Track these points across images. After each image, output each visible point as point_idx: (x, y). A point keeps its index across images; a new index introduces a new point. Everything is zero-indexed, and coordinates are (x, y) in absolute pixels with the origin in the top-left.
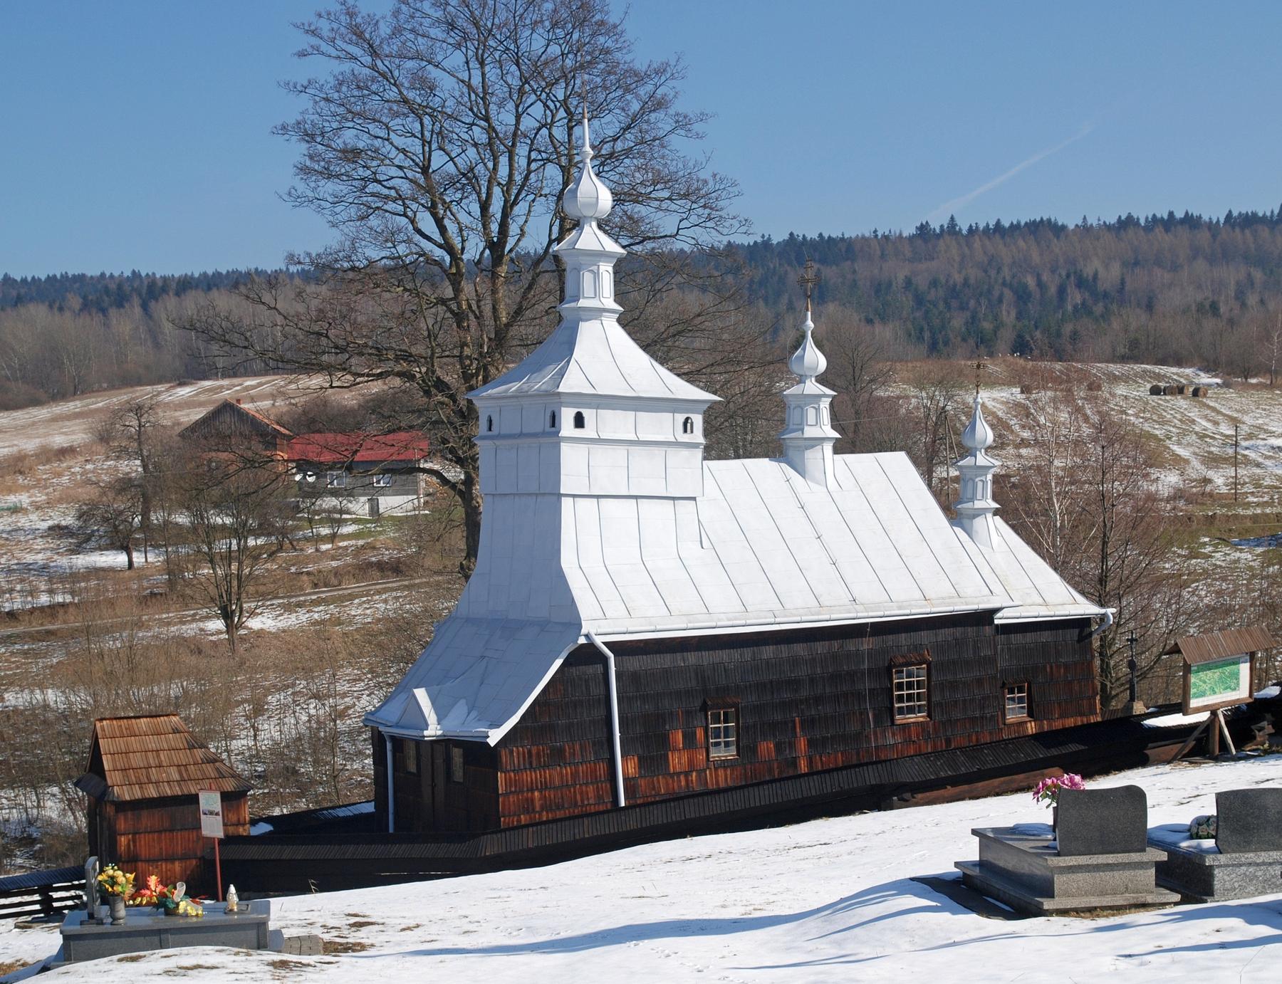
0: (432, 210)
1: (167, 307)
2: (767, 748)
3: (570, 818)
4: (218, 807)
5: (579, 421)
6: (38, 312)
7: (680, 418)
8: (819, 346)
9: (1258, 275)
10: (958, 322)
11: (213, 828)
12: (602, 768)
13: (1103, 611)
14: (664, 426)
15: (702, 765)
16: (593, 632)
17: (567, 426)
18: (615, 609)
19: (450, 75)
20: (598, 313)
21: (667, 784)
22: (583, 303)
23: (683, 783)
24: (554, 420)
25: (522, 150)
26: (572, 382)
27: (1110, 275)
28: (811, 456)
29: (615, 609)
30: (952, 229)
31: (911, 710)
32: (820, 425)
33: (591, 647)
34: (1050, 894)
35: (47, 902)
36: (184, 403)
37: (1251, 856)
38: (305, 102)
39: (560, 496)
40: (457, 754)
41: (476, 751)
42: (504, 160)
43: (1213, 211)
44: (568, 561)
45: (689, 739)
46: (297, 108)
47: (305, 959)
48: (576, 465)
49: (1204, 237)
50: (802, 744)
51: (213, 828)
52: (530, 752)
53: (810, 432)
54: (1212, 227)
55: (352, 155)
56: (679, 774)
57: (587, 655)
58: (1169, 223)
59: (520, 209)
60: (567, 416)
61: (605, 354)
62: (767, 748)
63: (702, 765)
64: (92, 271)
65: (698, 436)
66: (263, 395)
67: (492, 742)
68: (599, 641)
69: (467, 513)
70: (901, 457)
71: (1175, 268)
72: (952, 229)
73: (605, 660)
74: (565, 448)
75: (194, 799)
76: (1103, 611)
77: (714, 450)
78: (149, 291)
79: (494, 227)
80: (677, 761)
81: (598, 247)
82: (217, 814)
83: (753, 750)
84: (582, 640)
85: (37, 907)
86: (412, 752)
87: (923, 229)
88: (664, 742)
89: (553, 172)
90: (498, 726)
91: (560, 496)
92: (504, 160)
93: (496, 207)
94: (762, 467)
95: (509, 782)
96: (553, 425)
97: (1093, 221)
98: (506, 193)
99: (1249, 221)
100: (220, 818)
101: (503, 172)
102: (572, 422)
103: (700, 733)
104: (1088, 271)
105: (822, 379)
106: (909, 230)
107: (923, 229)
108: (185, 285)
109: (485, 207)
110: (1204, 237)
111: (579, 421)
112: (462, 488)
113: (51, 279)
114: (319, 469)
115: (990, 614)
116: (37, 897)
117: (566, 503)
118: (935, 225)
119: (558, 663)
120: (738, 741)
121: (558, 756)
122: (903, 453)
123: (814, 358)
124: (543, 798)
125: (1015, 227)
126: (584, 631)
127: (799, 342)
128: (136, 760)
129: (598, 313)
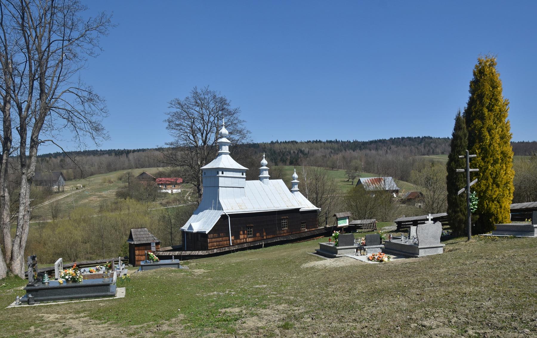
0: (193, 135)
1: (131, 156)
6: (107, 156)
9: (333, 151)
10: (279, 158)
14: (239, 175)
19: (195, 111)
25: (210, 125)
27: (306, 150)
30: (277, 142)
32: (266, 174)
34: (337, 254)
36: (137, 172)
37: (372, 246)
38: (169, 116)
40: (199, 236)
42: (206, 126)
43: (324, 140)
46: (167, 117)
49: (322, 144)
54: (324, 143)
55: (178, 125)
58: (316, 142)
59: (209, 135)
61: (225, 161)
64: (117, 149)
65: (244, 176)
66: (151, 171)
67: (207, 233)
69: (472, 103)
70: (281, 180)
71: (318, 150)
72: (277, 142)
77: (247, 179)
78: (128, 152)
79: (204, 138)
86: (190, 236)
87: (272, 142)
88: (239, 234)
89: (215, 128)
92: (206, 126)
93: (204, 136)
94: (257, 182)
97: (303, 141)
98: (206, 131)
99: (331, 142)
101: (206, 128)
104: (303, 149)
105: (266, 166)
106: (269, 142)
107: (272, 142)
108: (134, 151)
109: (202, 134)
110: (322, 144)
113: (109, 150)
118: (274, 141)
122: (281, 181)
125: (289, 142)
127: (263, 158)
128: (139, 236)
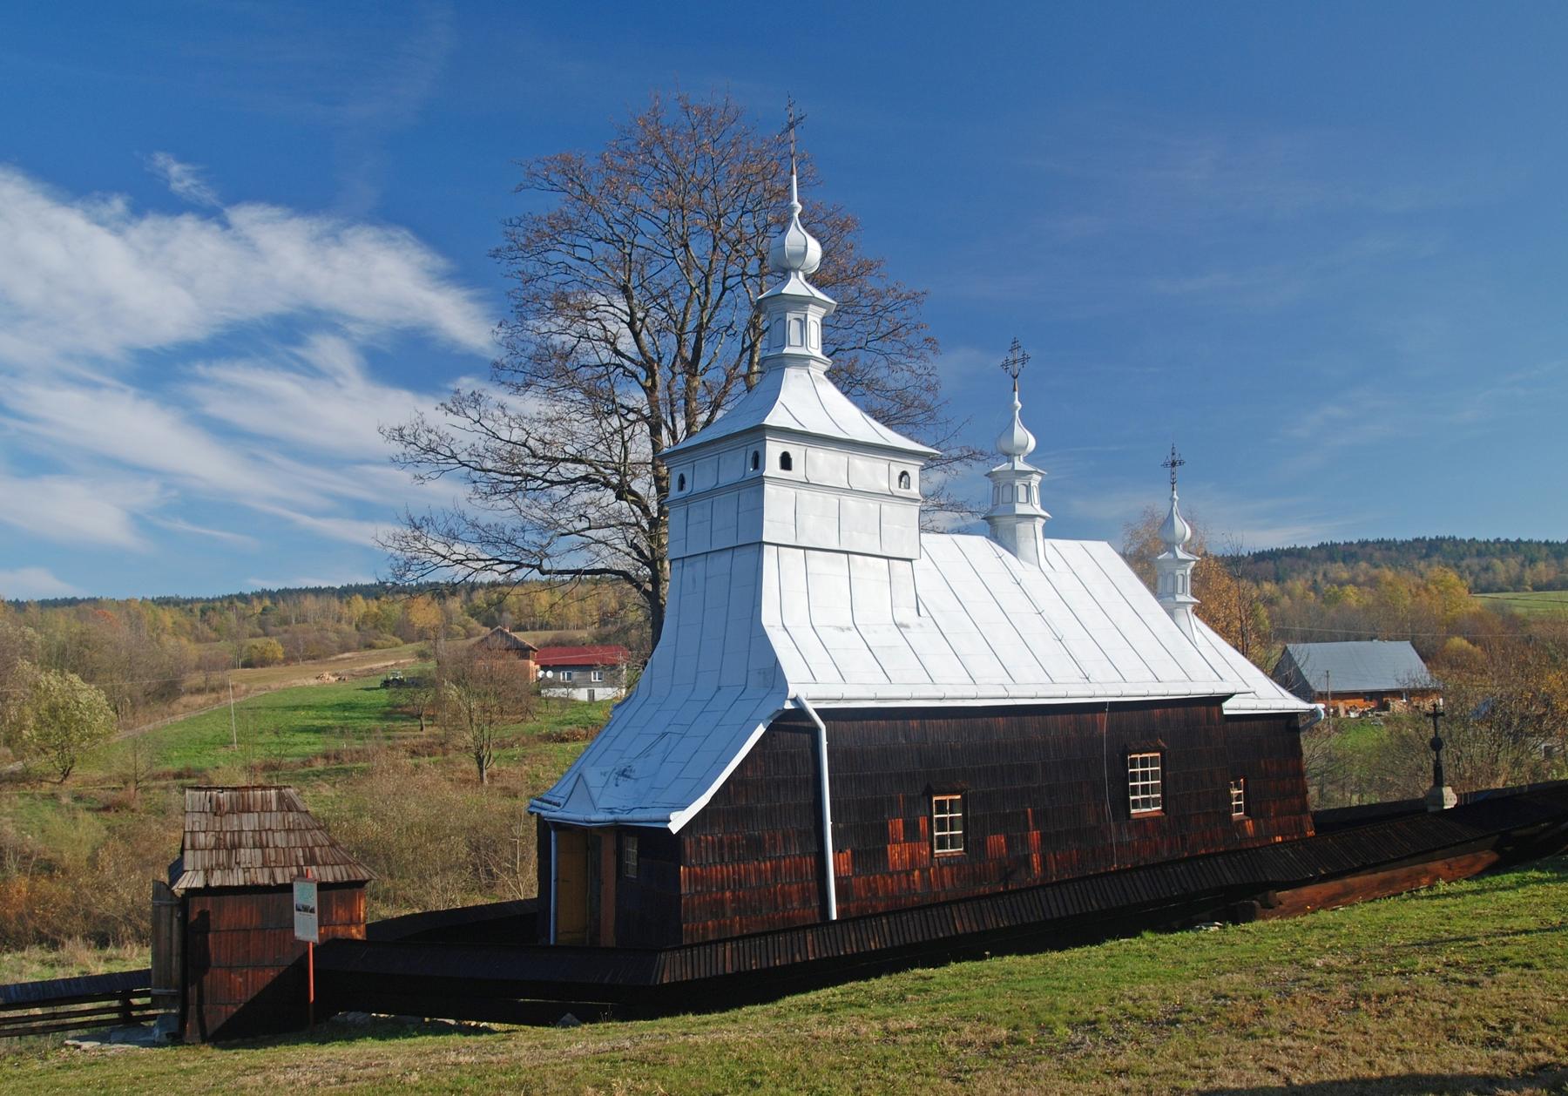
2: (996, 841)
3: (296, 708)
4: (313, 903)
5: (786, 462)
7: (896, 470)
8: (1027, 425)
11: (307, 930)
12: (810, 861)
13: (1313, 706)
14: (875, 473)
15: (925, 863)
16: (802, 696)
17: (772, 466)
18: (827, 673)
20: (803, 361)
21: (886, 883)
22: (787, 350)
23: (904, 885)
24: (758, 460)
26: (775, 418)
28: (1023, 528)
29: (827, 673)
31: (1146, 803)
33: (800, 712)
35: (127, 1008)
39: (761, 544)
41: (655, 840)
44: (769, 617)
45: (911, 832)
47: (495, 1026)
48: (780, 508)
50: (1035, 835)
51: (307, 930)
52: (721, 841)
53: (1021, 509)
56: (899, 873)
57: (792, 724)
60: (773, 450)
61: (808, 399)
62: (996, 841)
63: (925, 863)
68: (810, 707)
73: (815, 731)
74: (769, 489)
75: (288, 888)
76: (1313, 706)
80: (897, 853)
81: (806, 293)
82: (312, 911)
83: (982, 844)
84: (788, 706)
85: (115, 1016)
88: (883, 836)
90: (683, 807)
91: (761, 544)
95: (695, 879)
96: (756, 466)
100: (315, 916)
102: (777, 463)
103: (923, 823)
111: (786, 462)
112: (649, 587)
114: (556, 668)
115: (1218, 700)
116: (115, 1003)
117: (769, 554)
119: (760, 730)
120: (965, 835)
121: (756, 847)
123: (1024, 437)
124: (736, 899)
126: (791, 694)
129: (803, 361)
